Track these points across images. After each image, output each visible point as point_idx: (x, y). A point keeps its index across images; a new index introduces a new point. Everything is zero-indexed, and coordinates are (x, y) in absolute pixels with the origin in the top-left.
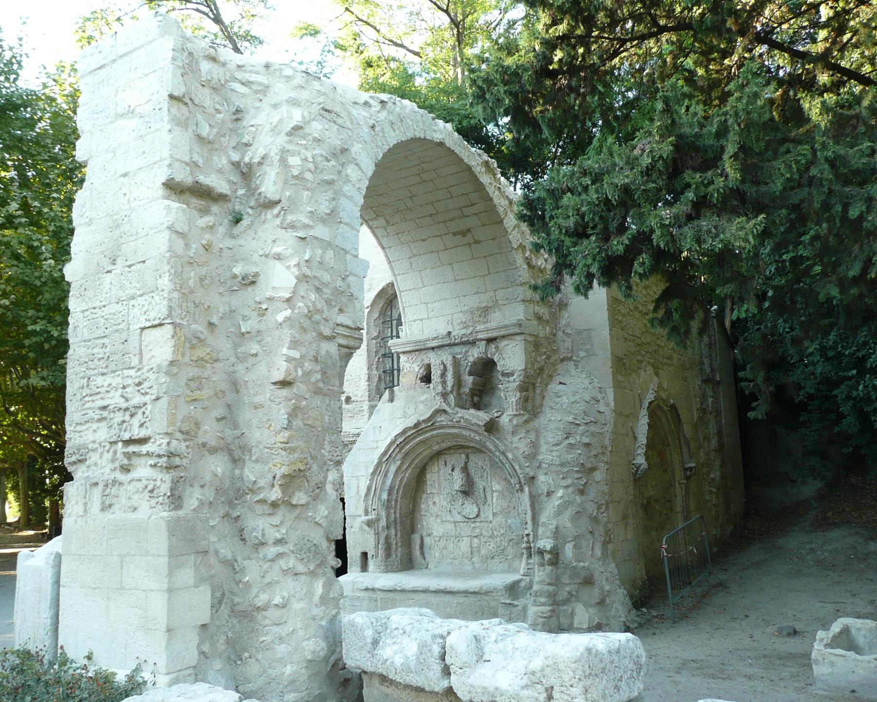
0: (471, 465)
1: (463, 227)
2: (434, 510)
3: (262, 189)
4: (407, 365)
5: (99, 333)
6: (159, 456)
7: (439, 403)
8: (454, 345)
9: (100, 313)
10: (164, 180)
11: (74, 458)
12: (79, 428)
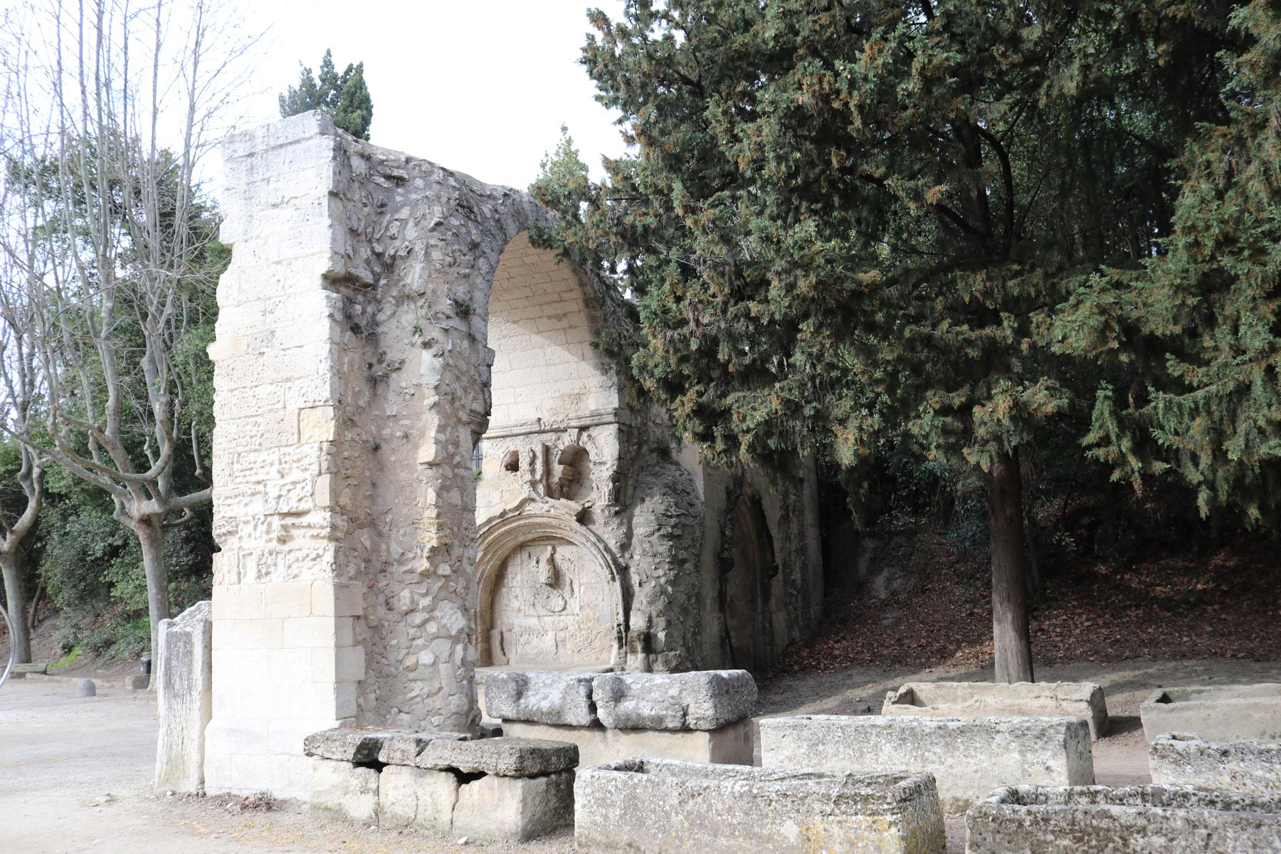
0: (558, 557)
1: (560, 311)
2: (515, 604)
3: (408, 281)
4: (491, 452)
5: (249, 412)
6: (322, 527)
7: (526, 492)
8: (544, 432)
9: (251, 393)
10: (324, 271)
11: (223, 530)
12: (228, 502)
